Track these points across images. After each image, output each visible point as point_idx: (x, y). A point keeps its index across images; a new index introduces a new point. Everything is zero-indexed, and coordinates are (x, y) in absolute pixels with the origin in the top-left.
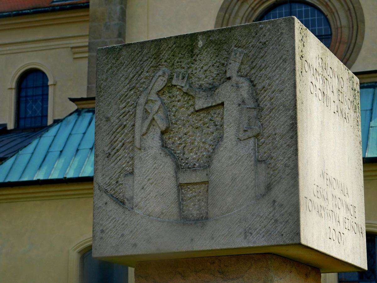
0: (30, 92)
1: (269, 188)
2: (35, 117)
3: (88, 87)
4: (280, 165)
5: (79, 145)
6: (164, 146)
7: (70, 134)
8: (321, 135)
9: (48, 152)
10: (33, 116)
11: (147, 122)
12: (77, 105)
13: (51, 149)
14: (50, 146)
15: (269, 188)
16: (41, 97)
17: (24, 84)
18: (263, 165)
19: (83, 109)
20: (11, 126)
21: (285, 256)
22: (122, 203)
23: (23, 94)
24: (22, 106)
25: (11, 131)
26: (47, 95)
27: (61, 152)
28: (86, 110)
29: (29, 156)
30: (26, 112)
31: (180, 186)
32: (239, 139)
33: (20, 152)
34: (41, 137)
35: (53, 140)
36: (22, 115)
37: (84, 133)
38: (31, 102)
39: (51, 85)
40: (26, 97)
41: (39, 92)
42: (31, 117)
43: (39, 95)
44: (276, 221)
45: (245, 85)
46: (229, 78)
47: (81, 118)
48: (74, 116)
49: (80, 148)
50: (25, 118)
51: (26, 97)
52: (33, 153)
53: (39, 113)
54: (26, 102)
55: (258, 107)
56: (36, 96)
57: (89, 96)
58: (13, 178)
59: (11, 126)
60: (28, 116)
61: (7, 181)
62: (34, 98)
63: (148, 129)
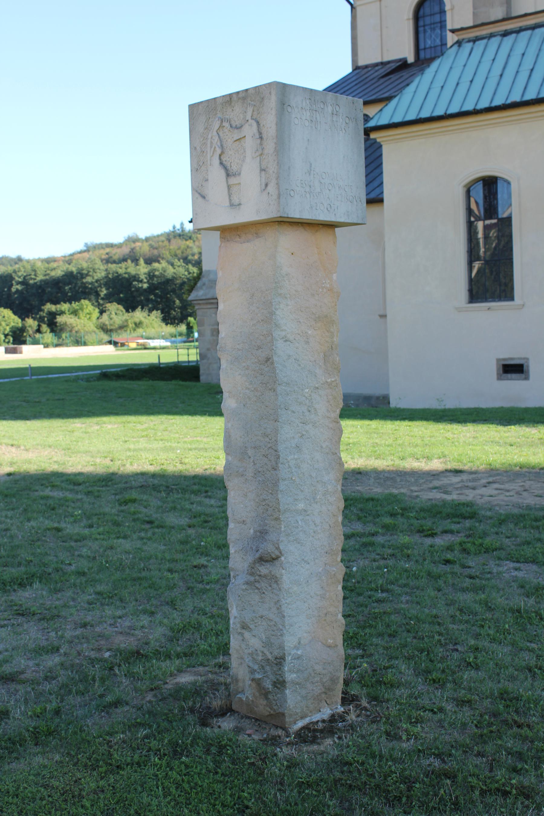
0: (428, 20)
1: (266, 185)
2: (435, 47)
3: (474, 13)
4: (271, 172)
5: (460, 78)
6: (221, 163)
7: (451, 68)
8: (306, 148)
9: (429, 88)
10: (432, 45)
11: (213, 149)
12: (457, 35)
13: (433, 86)
14: (432, 83)
15: (266, 185)
16: (439, 25)
17: (421, 13)
18: (264, 172)
19: (463, 39)
20: (411, 59)
21: (308, 221)
22: (204, 197)
23: (421, 23)
24: (421, 36)
25: (411, 65)
26: (445, 21)
27: (442, 87)
28: (467, 40)
29: (412, 94)
30: (425, 42)
31: (229, 187)
32: (253, 158)
33: (404, 92)
34: (422, 74)
35: (435, 76)
36: (422, 46)
37: (465, 66)
38: (429, 31)
39: (449, 10)
40: (424, 26)
41: (437, 18)
42: (431, 47)
43: (437, 23)
44: (270, 204)
45: (255, 124)
46: (247, 121)
47: (461, 48)
48: (455, 48)
49: (461, 81)
50: (425, 49)
51: (424, 26)
52: (415, 92)
53: (438, 42)
54: (425, 31)
55: (261, 138)
56: (434, 23)
57: (479, 22)
58: (397, 119)
59: (411, 59)
60: (427, 46)
61: (391, 122)
62: (432, 26)
63: (213, 153)
